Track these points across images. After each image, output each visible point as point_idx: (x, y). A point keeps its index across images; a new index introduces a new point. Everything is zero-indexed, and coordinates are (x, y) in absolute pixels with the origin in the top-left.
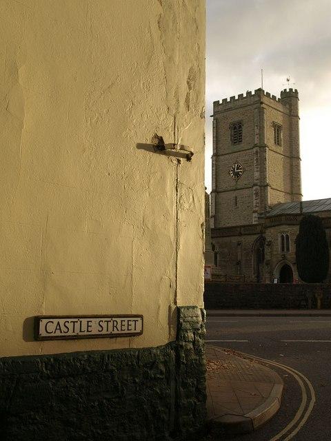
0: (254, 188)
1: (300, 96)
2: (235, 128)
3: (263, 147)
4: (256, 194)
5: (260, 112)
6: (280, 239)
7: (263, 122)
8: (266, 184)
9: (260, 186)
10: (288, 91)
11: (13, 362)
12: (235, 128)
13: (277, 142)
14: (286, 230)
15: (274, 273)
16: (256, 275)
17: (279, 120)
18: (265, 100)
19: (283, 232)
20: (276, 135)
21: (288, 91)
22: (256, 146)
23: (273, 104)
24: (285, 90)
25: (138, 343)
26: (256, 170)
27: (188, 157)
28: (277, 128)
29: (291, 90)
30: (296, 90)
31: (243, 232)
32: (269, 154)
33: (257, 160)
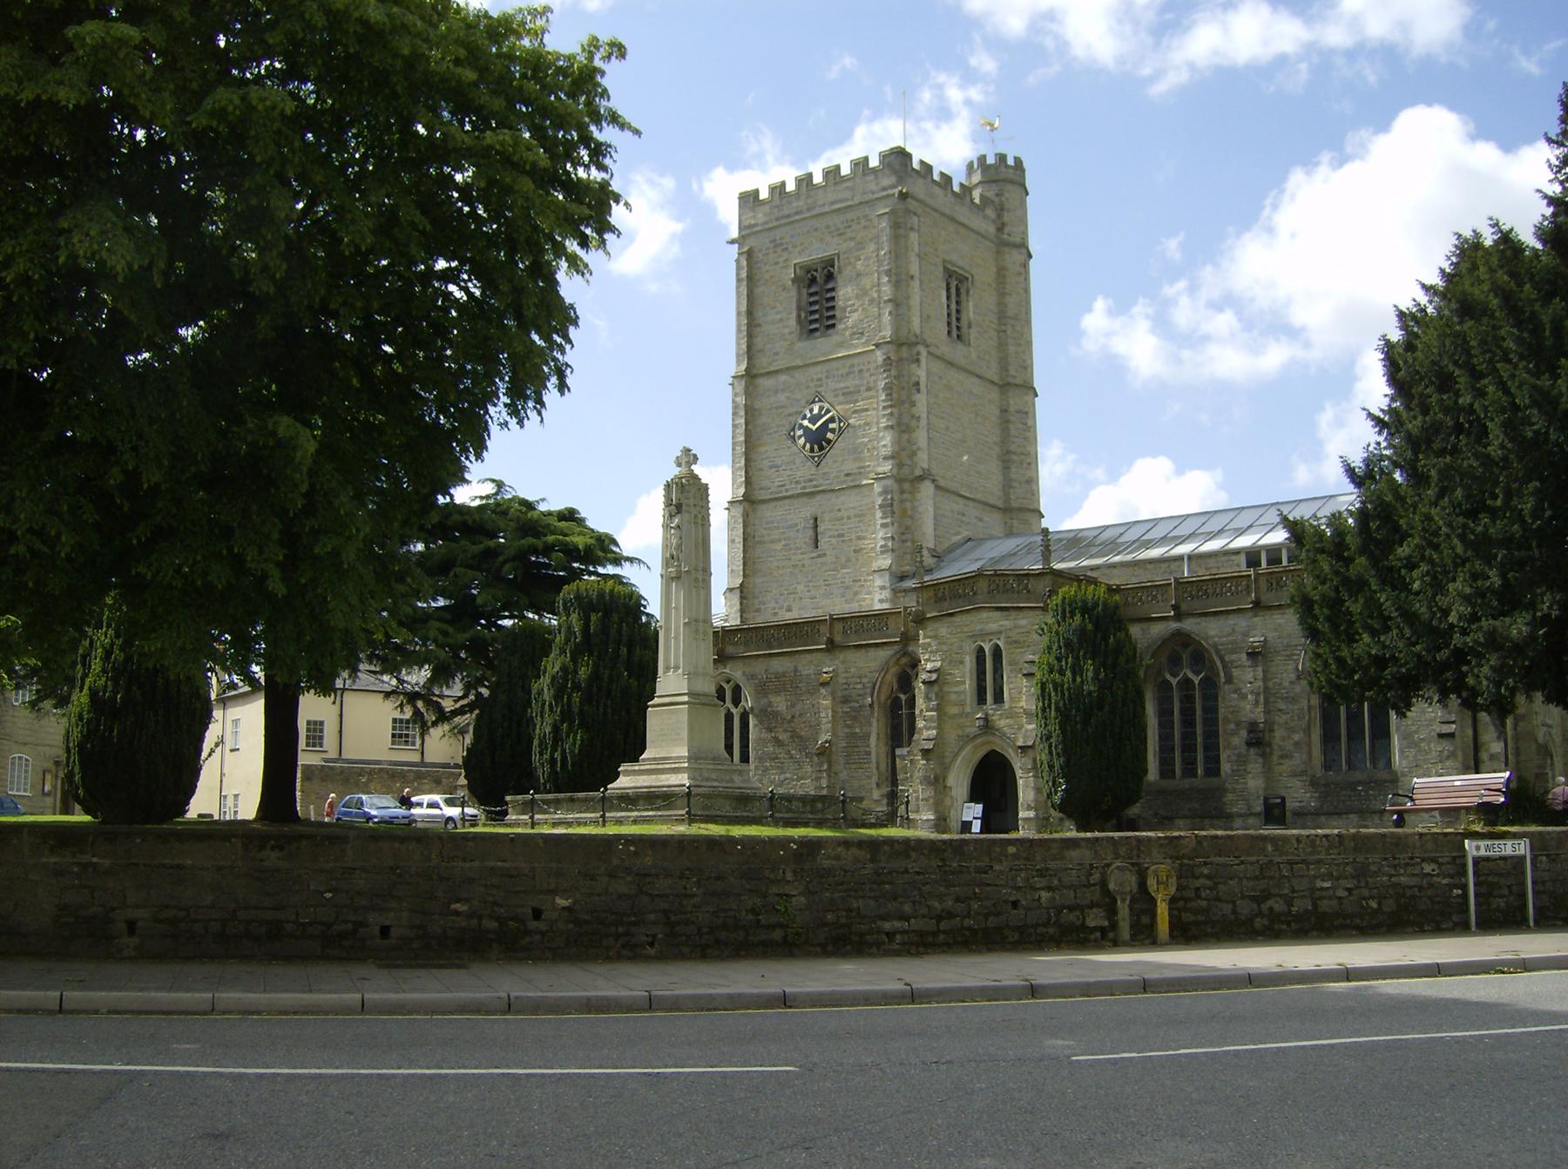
2: (813, 281)
6: (969, 662)
8: (918, 472)
14: (993, 627)
16: (886, 789)
19: (983, 635)
20: (954, 306)
27: (816, 519)
29: (1002, 158)
30: (1018, 161)
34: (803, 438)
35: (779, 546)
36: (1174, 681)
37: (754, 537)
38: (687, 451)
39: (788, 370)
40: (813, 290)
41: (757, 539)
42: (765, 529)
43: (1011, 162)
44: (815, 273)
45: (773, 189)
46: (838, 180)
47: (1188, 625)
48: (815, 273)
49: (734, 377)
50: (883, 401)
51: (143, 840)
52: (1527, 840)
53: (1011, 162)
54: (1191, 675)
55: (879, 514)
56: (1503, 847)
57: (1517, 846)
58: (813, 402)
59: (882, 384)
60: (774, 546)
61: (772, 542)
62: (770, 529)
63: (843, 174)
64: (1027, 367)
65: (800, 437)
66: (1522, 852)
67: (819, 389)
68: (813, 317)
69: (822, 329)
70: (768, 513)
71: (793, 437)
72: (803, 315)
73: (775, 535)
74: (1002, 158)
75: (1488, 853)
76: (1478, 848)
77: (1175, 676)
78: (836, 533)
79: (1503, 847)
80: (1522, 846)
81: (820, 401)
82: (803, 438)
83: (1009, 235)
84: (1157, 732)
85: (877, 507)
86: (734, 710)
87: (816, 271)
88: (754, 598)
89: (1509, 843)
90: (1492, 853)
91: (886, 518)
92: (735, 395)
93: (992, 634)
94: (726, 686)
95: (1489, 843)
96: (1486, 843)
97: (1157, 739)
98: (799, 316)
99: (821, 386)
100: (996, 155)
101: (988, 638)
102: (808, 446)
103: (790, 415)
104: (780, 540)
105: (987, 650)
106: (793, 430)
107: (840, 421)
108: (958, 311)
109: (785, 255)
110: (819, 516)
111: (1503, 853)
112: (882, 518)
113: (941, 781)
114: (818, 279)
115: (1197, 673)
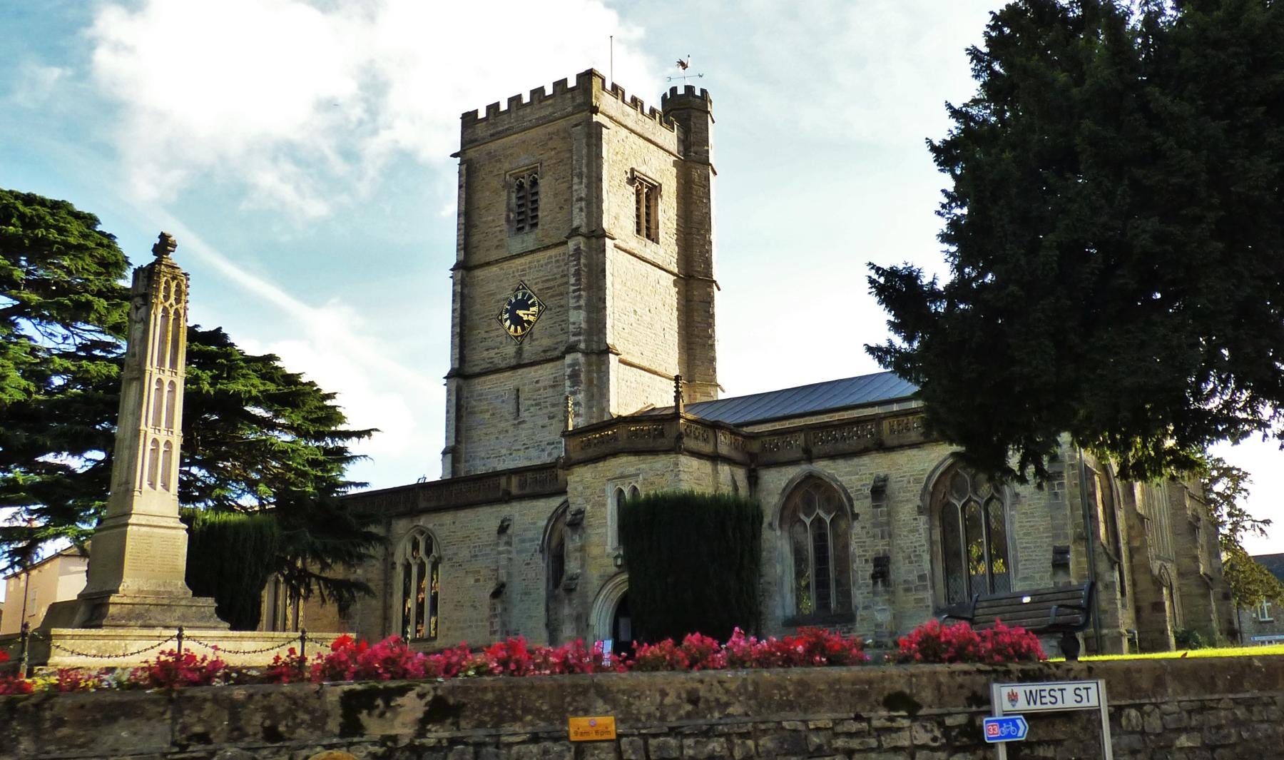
0: (569, 359)
1: (714, 109)
2: (521, 186)
3: (597, 236)
4: (574, 377)
5: (589, 136)
7: (600, 167)
8: (603, 347)
9: (586, 353)
10: (681, 91)
11: (37, 290)
12: (521, 186)
13: (646, 226)
14: (632, 470)
15: (593, 619)
17: (663, 170)
18: (606, 102)
20: (643, 210)
21: (681, 91)
22: (575, 232)
23: (631, 117)
24: (674, 90)
25: (136, 493)
26: (572, 302)
27: (518, 390)
28: (647, 194)
29: (689, 89)
30: (703, 91)
31: (515, 490)
32: (614, 261)
33: (577, 274)
34: (509, 321)
35: (487, 416)
36: (808, 522)
37: (467, 409)
38: (164, 237)
39: (497, 262)
40: (521, 194)
41: (469, 410)
42: (475, 400)
43: (698, 93)
44: (522, 180)
45: (489, 108)
46: (542, 97)
47: (823, 467)
48: (522, 180)
49: (451, 270)
50: (573, 285)
51: (789, 645)
52: (1102, 683)
53: (698, 93)
54: (822, 515)
55: (568, 383)
56: (1058, 694)
57: (1083, 693)
58: (518, 289)
59: (572, 270)
60: (482, 416)
61: (481, 413)
62: (480, 400)
63: (547, 94)
64: (708, 264)
65: (506, 320)
66: (1093, 702)
67: (523, 278)
68: (520, 218)
69: (527, 228)
70: (485, 386)
71: (501, 321)
72: (512, 216)
73: (484, 405)
74: (689, 89)
75: (1032, 706)
76: (1013, 698)
77: (807, 515)
78: (534, 403)
79: (1058, 694)
80: (1093, 692)
81: (524, 288)
82: (509, 321)
83: (696, 153)
84: (793, 569)
85: (566, 377)
86: (426, 561)
87: (523, 178)
88: (466, 462)
89: (1070, 688)
90: (1039, 706)
91: (573, 387)
92: (454, 284)
93: (630, 476)
94: (419, 537)
95: (1034, 687)
96: (1028, 689)
97: (794, 576)
98: (508, 216)
99: (524, 275)
100: (685, 86)
101: (627, 481)
102: (513, 327)
103: (498, 301)
104: (488, 411)
105: (626, 493)
106: (501, 314)
107: (540, 305)
108: (648, 214)
109: (498, 165)
110: (521, 388)
111: (1059, 705)
112: (570, 387)
113: (584, 619)
114: (525, 185)
115: (828, 513)
